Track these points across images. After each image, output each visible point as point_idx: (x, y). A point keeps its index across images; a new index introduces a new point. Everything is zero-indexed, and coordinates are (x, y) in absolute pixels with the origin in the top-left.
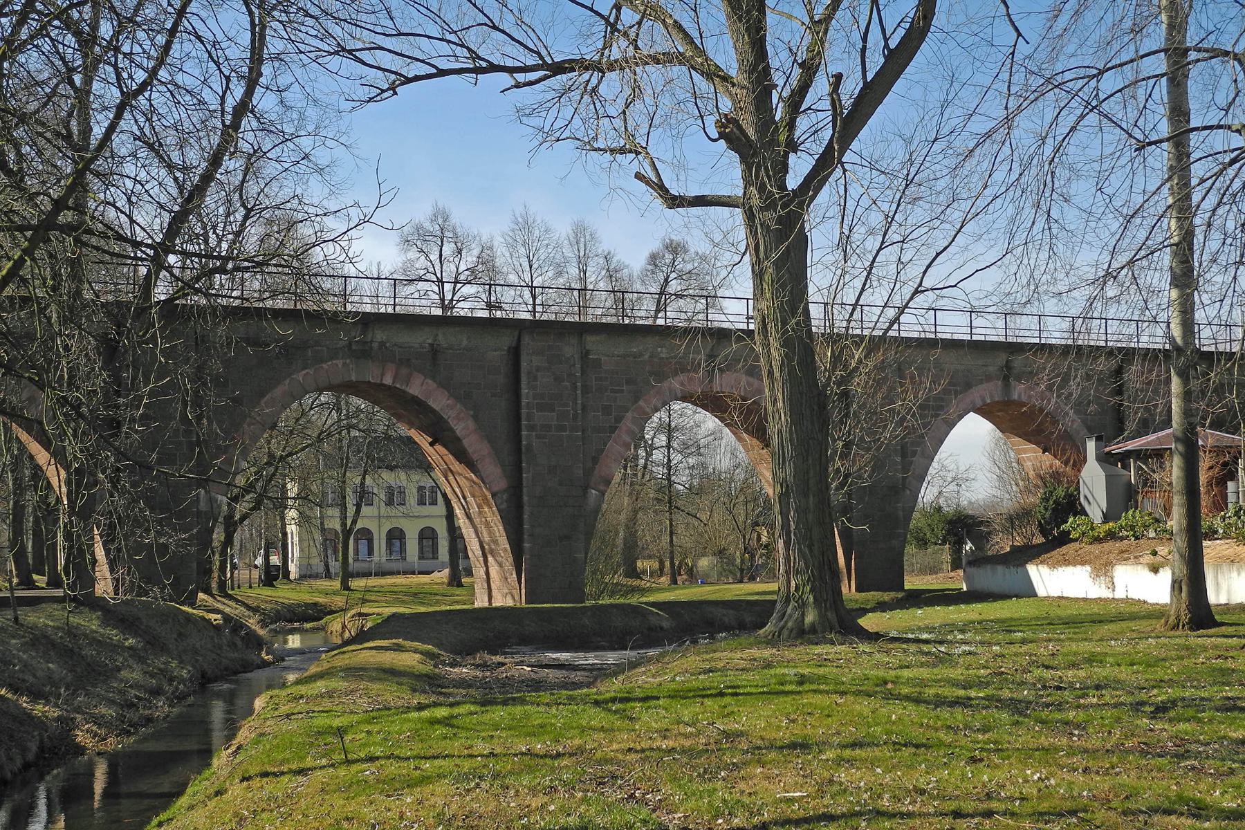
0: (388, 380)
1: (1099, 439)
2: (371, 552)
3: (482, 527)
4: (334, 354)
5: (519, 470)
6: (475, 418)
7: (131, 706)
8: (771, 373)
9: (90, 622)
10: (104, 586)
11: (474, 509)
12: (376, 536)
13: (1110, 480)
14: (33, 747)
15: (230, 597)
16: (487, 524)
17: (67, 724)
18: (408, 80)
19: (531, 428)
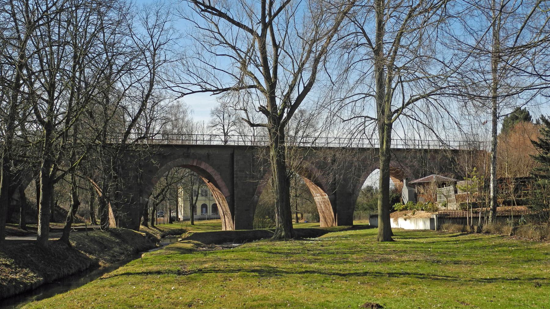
0: (195, 164)
1: (407, 179)
2: (206, 211)
3: (223, 207)
4: (179, 157)
5: (233, 190)
6: (220, 175)
7: (115, 257)
8: (274, 171)
9: (107, 236)
10: (112, 223)
11: (221, 202)
12: (208, 207)
13: (410, 192)
14: (88, 265)
15: (155, 227)
16: (224, 206)
17: (97, 260)
18: (185, 94)
19: (237, 177)
